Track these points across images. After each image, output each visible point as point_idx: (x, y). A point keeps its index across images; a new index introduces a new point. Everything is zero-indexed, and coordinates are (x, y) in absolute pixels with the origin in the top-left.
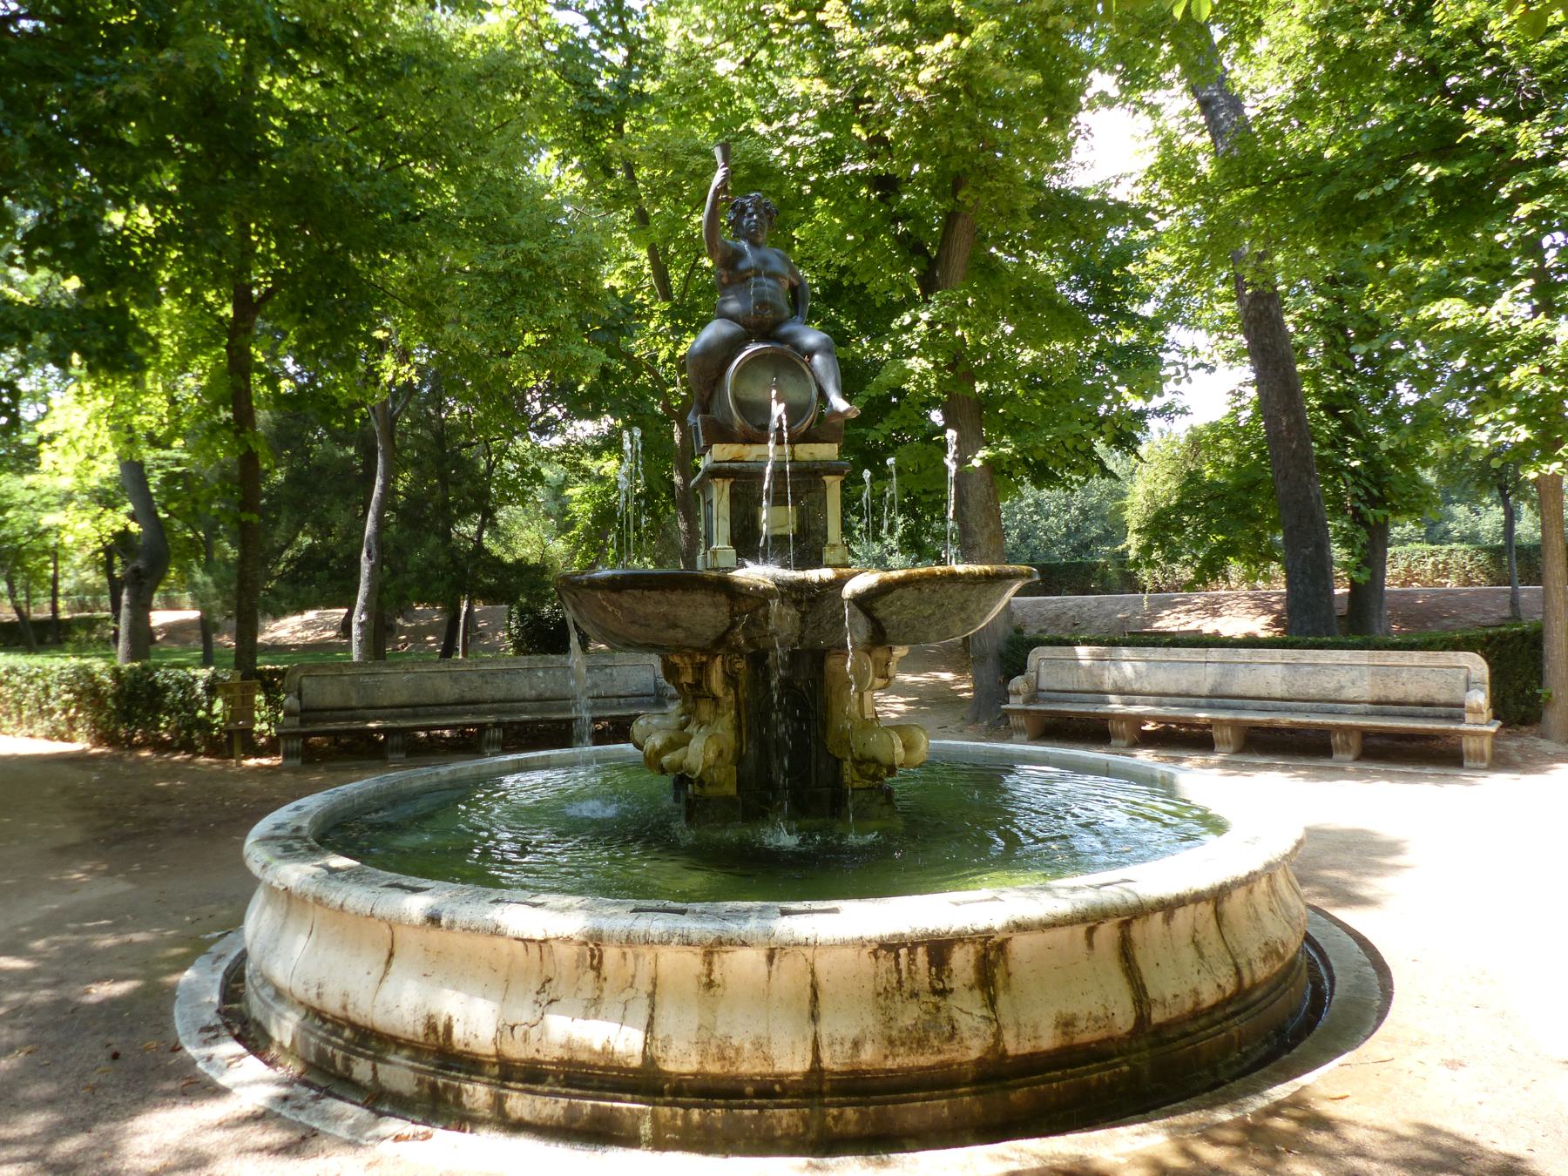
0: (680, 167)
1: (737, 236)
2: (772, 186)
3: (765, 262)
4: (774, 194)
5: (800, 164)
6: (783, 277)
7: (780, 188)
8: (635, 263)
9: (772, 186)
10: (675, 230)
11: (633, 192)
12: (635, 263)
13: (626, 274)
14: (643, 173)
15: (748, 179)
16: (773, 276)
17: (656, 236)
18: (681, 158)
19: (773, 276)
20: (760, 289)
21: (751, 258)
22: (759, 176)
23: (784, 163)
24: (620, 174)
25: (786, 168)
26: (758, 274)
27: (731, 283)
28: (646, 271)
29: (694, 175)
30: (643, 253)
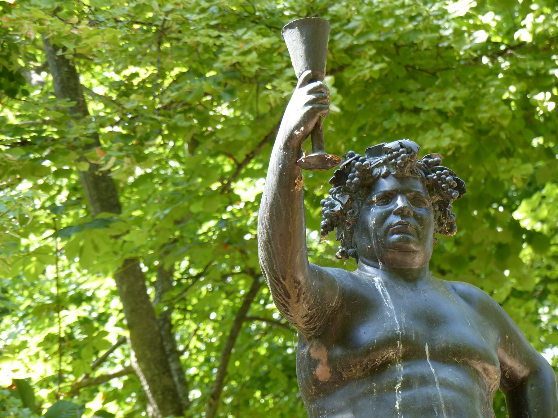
0: (200, 59)
1: (352, 254)
2: (451, 98)
3: (432, 320)
4: (454, 118)
5: (524, 35)
6: (486, 358)
7: (472, 103)
8: (83, 311)
9: (451, 98)
10: (185, 221)
11: (76, 130)
12: (83, 311)
13: (64, 344)
14: (96, 80)
15: (385, 83)
16: (456, 355)
17: (137, 237)
18: (204, 37)
19: (456, 355)
20: (417, 391)
21: (392, 313)
22: (413, 72)
23: (481, 37)
24: (41, 80)
25: (492, 50)
26: (413, 354)
27: (339, 380)
28: (113, 331)
29: (236, 80)
30: (103, 286)
